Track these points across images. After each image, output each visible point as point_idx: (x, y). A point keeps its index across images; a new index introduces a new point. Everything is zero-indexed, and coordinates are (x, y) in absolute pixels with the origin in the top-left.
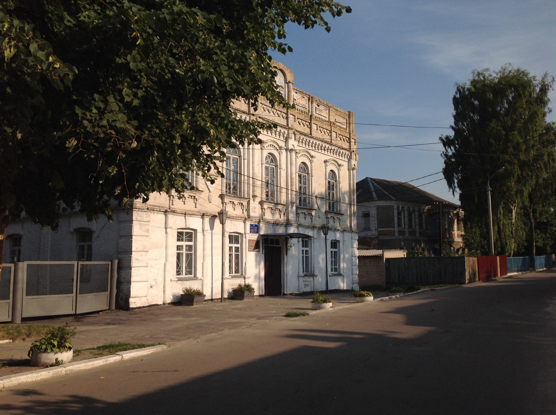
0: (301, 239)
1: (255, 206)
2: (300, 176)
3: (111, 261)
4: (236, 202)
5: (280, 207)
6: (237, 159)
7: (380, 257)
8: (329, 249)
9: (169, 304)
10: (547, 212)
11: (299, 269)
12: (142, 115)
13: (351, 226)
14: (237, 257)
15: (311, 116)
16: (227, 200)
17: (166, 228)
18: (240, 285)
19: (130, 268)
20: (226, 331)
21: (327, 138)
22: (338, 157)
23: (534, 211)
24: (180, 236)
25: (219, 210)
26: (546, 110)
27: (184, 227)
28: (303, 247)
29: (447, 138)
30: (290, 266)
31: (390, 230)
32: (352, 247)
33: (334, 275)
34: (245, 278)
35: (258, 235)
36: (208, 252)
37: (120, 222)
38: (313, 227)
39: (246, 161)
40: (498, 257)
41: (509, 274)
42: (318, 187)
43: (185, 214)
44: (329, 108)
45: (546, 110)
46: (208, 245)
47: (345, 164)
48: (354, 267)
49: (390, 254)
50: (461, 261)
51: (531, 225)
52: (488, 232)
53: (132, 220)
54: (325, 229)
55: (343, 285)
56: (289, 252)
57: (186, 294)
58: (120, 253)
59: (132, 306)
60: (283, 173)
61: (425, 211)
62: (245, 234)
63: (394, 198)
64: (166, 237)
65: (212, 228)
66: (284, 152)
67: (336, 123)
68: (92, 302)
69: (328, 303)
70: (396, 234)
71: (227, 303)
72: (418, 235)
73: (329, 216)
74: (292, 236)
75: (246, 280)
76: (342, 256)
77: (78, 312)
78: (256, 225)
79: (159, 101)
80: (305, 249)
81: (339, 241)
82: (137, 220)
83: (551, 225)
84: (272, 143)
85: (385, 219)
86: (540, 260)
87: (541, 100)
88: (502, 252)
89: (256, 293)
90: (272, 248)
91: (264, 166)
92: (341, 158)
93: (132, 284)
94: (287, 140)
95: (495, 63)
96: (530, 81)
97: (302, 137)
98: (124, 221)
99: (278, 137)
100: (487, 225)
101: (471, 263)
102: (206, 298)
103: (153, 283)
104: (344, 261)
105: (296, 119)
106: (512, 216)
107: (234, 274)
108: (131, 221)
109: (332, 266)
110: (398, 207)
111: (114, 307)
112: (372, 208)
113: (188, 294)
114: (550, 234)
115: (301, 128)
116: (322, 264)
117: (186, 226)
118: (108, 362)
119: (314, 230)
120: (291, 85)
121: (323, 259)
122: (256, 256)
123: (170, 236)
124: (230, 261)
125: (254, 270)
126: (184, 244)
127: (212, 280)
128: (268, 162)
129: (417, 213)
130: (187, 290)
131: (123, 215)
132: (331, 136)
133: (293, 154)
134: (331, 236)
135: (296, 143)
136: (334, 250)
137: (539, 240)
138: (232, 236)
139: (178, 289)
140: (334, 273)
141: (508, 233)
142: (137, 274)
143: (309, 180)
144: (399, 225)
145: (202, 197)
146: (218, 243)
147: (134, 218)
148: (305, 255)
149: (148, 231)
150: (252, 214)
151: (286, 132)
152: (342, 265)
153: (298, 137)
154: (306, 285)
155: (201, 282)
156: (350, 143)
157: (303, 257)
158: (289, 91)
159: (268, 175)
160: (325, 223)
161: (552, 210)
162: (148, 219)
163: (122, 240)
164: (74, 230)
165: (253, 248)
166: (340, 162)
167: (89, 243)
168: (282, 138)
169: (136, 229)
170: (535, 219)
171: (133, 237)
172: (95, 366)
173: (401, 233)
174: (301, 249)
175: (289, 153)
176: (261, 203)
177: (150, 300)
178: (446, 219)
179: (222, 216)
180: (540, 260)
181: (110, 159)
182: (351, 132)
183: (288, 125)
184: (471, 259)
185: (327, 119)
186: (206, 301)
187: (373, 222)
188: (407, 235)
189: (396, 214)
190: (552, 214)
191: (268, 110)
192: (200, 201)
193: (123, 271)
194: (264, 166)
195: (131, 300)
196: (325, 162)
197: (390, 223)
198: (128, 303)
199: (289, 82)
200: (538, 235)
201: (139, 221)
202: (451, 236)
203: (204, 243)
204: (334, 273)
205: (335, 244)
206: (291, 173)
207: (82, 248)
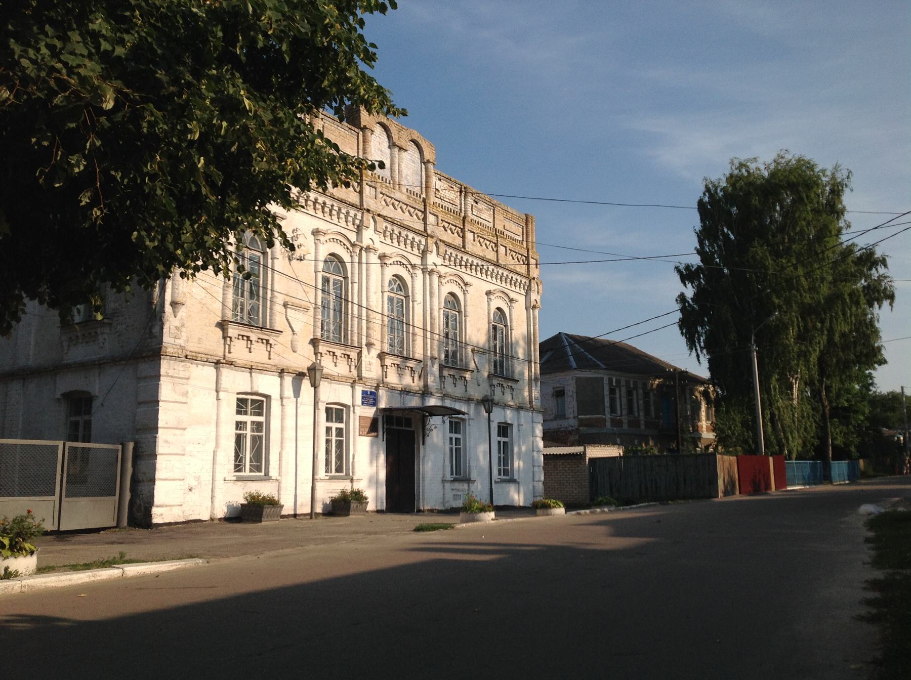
0: (446, 418)
1: (370, 359)
2: (447, 317)
3: (122, 444)
4: (339, 352)
5: (411, 364)
6: (341, 282)
7: (582, 456)
8: (495, 438)
9: (220, 519)
10: (848, 391)
11: (444, 471)
12: (127, 71)
13: (531, 402)
14: (339, 444)
15: (464, 218)
16: (322, 348)
17: (217, 391)
18: (343, 492)
19: (154, 456)
20: (312, 547)
21: (491, 256)
22: (508, 286)
23: (828, 389)
24: (242, 405)
25: (309, 364)
26: (842, 224)
27: (249, 391)
28: (451, 432)
29: (688, 267)
30: (430, 464)
31: (597, 419)
32: (534, 436)
33: (502, 481)
34: (352, 481)
35: (374, 409)
36: (290, 433)
37: (139, 379)
38: (469, 400)
39: (356, 286)
40: (771, 459)
41: (789, 488)
42: (476, 331)
43: (251, 369)
44: (494, 206)
45: (842, 224)
46: (290, 422)
47: (521, 299)
48: (536, 469)
49: (595, 452)
50: (709, 460)
51: (824, 410)
52: (755, 420)
53: (160, 375)
54: (488, 403)
55: (518, 497)
56: (428, 440)
57: (249, 503)
58: (138, 431)
59: (156, 520)
60: (418, 309)
61: (654, 386)
62: (354, 406)
63: (604, 367)
64: (218, 406)
65: (297, 392)
66: (419, 272)
67: (506, 232)
68: (87, 512)
69: (488, 513)
70: (608, 424)
71: (321, 521)
72: (643, 427)
73: (495, 382)
74: (433, 411)
75: (355, 484)
76: (516, 449)
77: (62, 529)
78: (371, 393)
79: (159, 51)
80: (454, 436)
81: (511, 425)
82: (168, 376)
83: (856, 412)
84: (399, 259)
85: (589, 400)
86: (839, 468)
87: (834, 209)
88: (778, 450)
89: (371, 507)
90: (399, 431)
91: (386, 295)
92: (513, 288)
93: (157, 483)
94: (424, 254)
95: (763, 155)
96: (819, 177)
97: (449, 251)
98: (145, 378)
99: (409, 249)
100: (753, 411)
101: (727, 465)
102: (284, 512)
103: (193, 483)
104: (519, 459)
105: (440, 221)
106: (792, 394)
107: (334, 473)
108: (158, 377)
109: (499, 465)
110: (610, 380)
111: (125, 522)
112: (569, 380)
113: (254, 503)
114: (854, 427)
115: (448, 237)
116: (483, 461)
117: (252, 388)
118: (98, 578)
119: (469, 405)
120: (431, 166)
121: (484, 452)
122: (372, 444)
123: (223, 404)
124: (328, 452)
125: (368, 468)
126: (248, 419)
127: (296, 480)
128: (392, 289)
129: (641, 391)
130: (252, 497)
131: (144, 368)
132: (497, 251)
133: (435, 278)
134: (498, 416)
135: (439, 261)
136: (503, 439)
137: (837, 435)
138: (331, 409)
139: (237, 495)
140: (502, 477)
141: (788, 421)
142: (165, 467)
143: (461, 323)
144: (613, 410)
145: (281, 343)
146: (306, 421)
147: (163, 371)
148: (454, 447)
149: (186, 394)
150: (365, 374)
151: (423, 242)
152: (516, 464)
153: (442, 250)
154: (456, 497)
155: (276, 484)
156: (528, 264)
157: (451, 449)
158: (427, 177)
159: (392, 311)
160: (489, 394)
161: (857, 387)
162: (186, 375)
163: (142, 409)
164: (64, 395)
165: (367, 430)
166: (512, 295)
167: (86, 418)
168: (416, 251)
169: (166, 390)
170: (830, 402)
171: (160, 404)
172: (74, 582)
173: (616, 423)
174: (449, 435)
175: (428, 276)
176: (381, 356)
177: (187, 513)
178: (689, 402)
179: (313, 374)
180: (839, 468)
181: (73, 143)
182: (530, 248)
183: (425, 230)
184: (726, 457)
185: (491, 225)
186: (283, 517)
187: (571, 404)
188: (625, 426)
189: (606, 392)
190: (856, 394)
191: (393, 204)
192: (276, 349)
193: (143, 462)
194: (386, 295)
195: (155, 510)
196: (488, 293)
197: (597, 406)
198: (149, 515)
199: (428, 161)
200: (835, 428)
201: (172, 377)
202: (696, 429)
203: (283, 419)
204: (502, 477)
205: (504, 429)
206: (431, 309)
207: (75, 425)
